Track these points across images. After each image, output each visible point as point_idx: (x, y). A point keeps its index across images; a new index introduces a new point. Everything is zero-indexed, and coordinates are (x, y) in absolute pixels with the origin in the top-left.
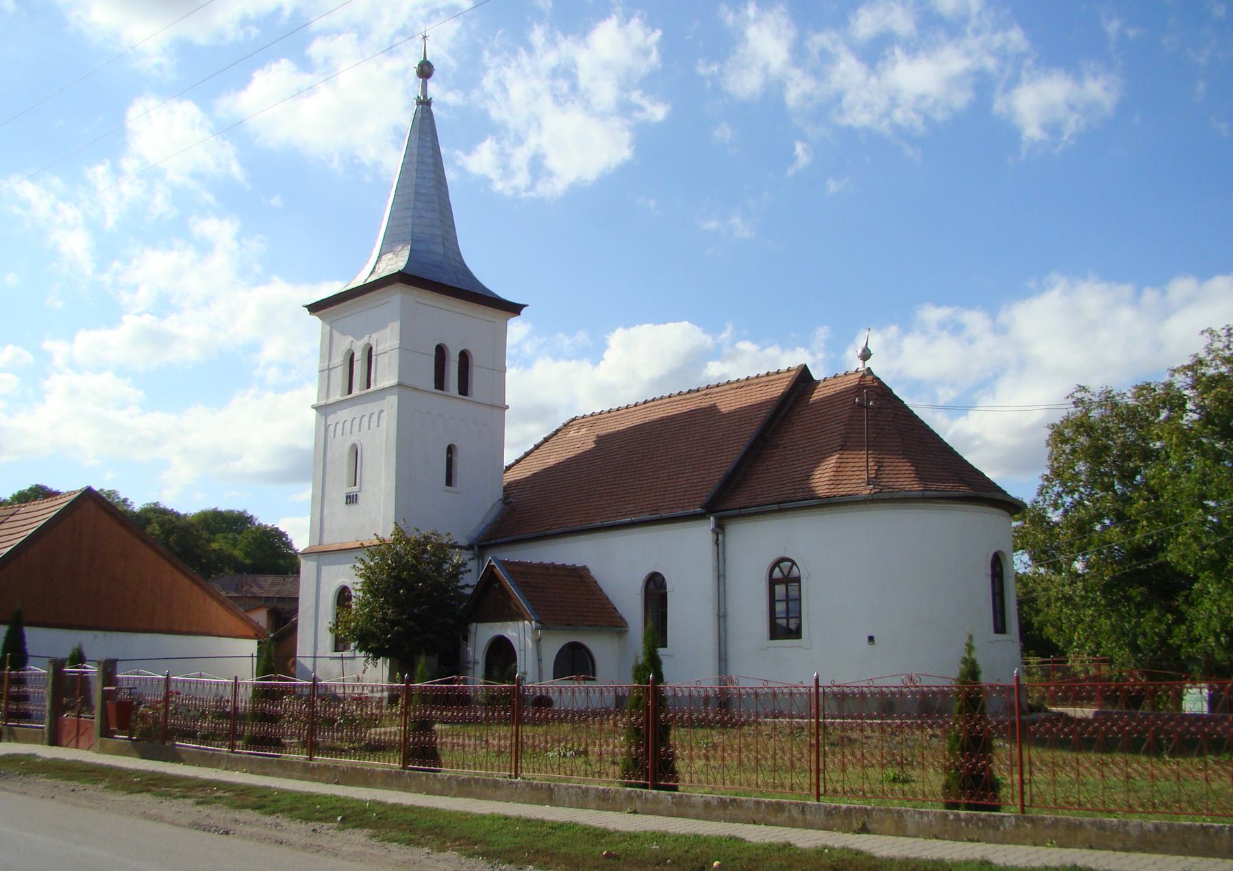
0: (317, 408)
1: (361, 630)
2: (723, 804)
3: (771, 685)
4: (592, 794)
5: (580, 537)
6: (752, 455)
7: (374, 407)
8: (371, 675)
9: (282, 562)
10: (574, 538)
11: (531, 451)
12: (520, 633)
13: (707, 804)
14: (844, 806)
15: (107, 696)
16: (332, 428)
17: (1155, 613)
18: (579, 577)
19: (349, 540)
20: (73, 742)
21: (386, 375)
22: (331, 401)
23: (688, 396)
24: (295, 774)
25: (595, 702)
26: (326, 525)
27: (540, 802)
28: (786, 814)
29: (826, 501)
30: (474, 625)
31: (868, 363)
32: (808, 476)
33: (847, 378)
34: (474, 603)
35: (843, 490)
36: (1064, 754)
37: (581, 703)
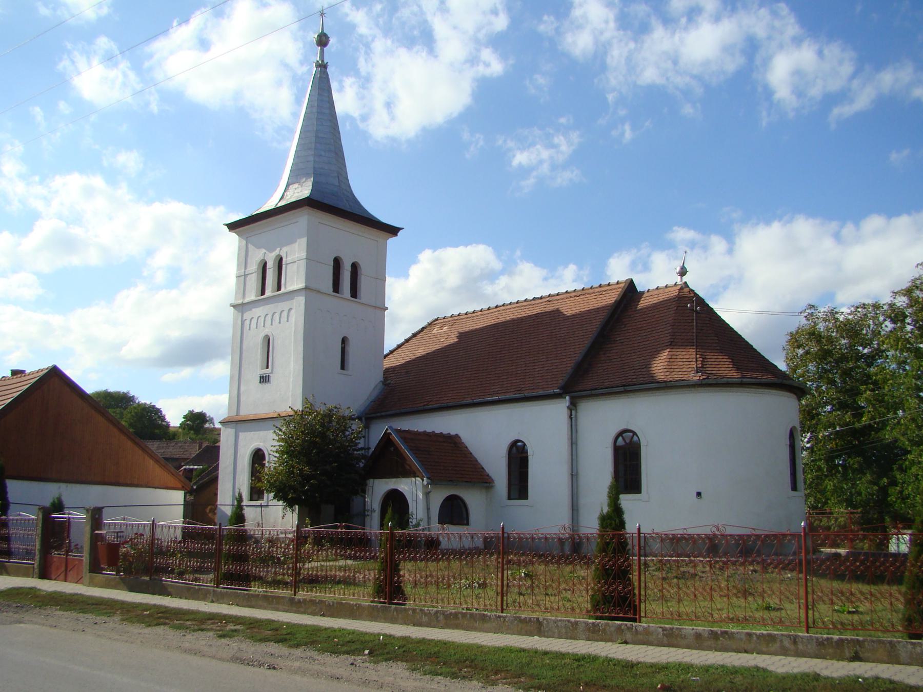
0: (234, 306)
1: (281, 482)
2: (714, 635)
4: (581, 627)
5: (452, 412)
6: (613, 344)
7: (284, 305)
8: (276, 519)
9: (157, 431)
10: (472, 409)
11: (403, 344)
12: (412, 488)
13: (698, 636)
14: (836, 637)
15: (95, 539)
16: (247, 322)
17: (869, 477)
18: (453, 442)
19: (263, 411)
20: (62, 576)
21: (295, 280)
22: (247, 300)
23: (533, 302)
24: (281, 607)
25: (467, 543)
26: (243, 399)
27: (530, 634)
28: (778, 644)
29: (663, 385)
30: (372, 480)
31: (685, 279)
32: (647, 366)
33: (667, 290)
34: (369, 466)
35: (676, 376)
36: (860, 586)
37: (455, 544)
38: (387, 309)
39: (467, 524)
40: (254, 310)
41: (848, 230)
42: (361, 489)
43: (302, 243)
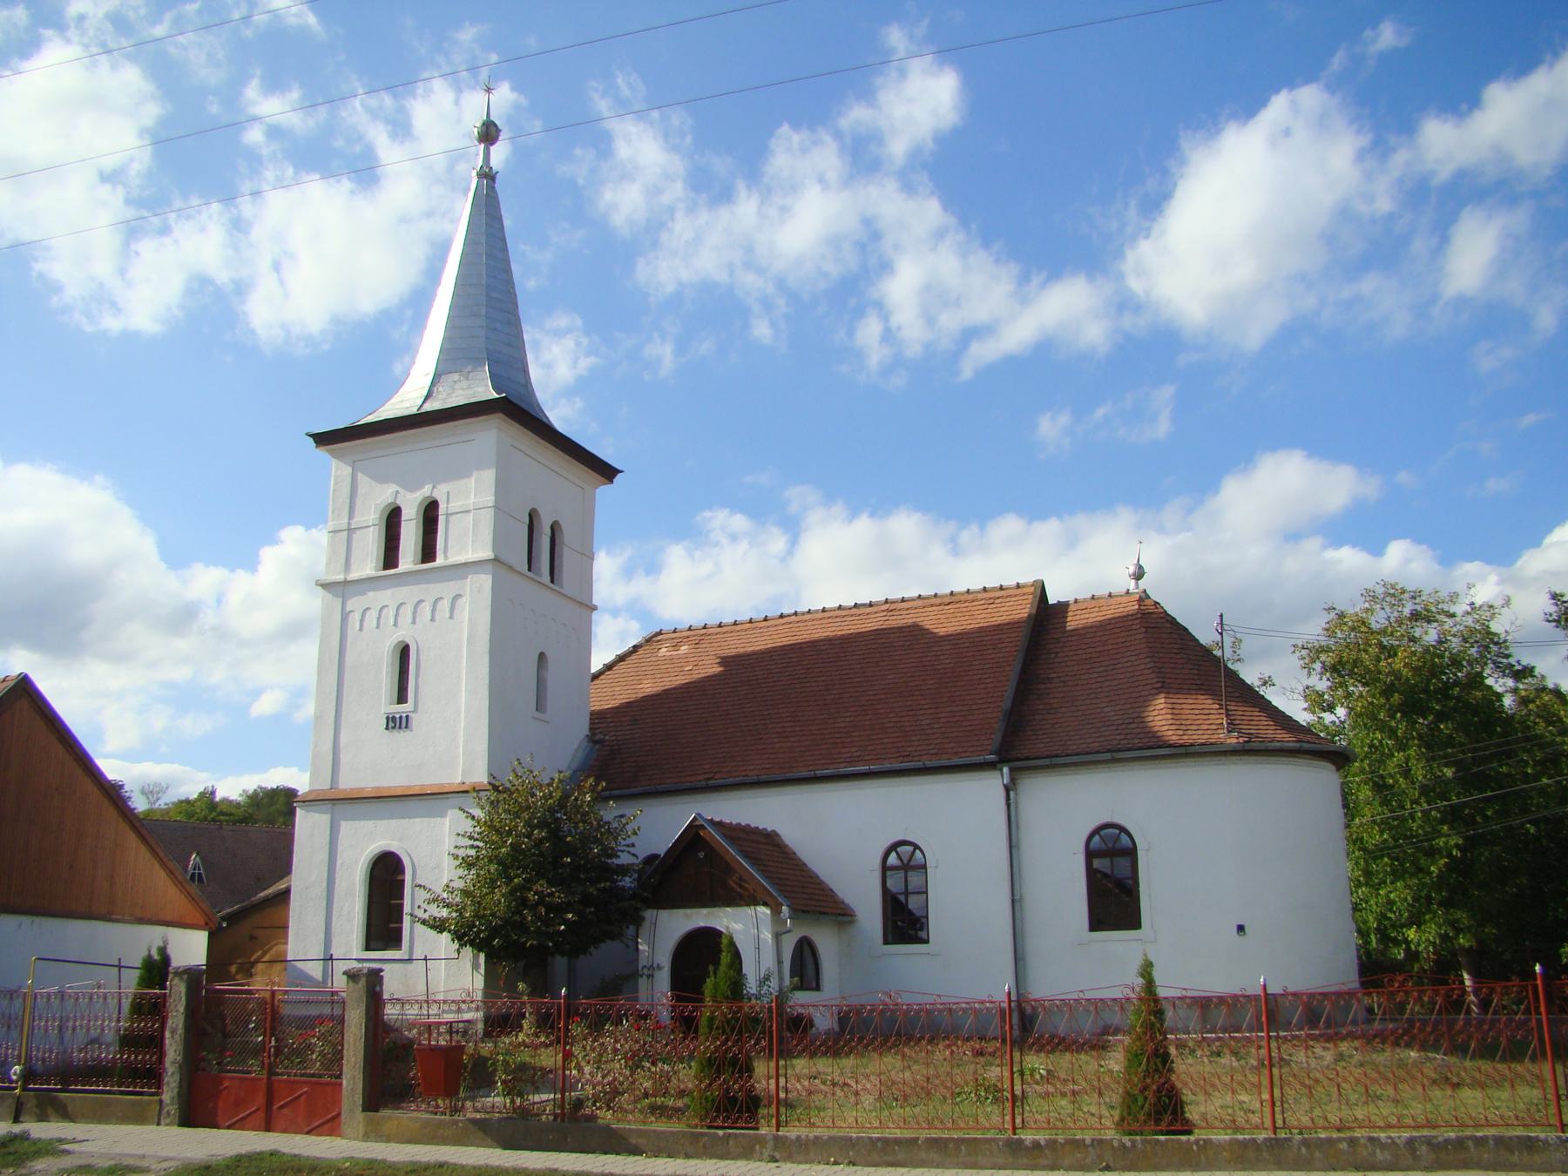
3: (944, 1000)
6: (1040, 689)
7: (446, 589)
16: (356, 616)
26: (344, 758)
29: (1182, 750)
32: (1140, 720)
33: (1112, 601)
38: (595, 608)
39: (818, 988)
40: (371, 594)
41: (966, 536)
43: (488, 477)
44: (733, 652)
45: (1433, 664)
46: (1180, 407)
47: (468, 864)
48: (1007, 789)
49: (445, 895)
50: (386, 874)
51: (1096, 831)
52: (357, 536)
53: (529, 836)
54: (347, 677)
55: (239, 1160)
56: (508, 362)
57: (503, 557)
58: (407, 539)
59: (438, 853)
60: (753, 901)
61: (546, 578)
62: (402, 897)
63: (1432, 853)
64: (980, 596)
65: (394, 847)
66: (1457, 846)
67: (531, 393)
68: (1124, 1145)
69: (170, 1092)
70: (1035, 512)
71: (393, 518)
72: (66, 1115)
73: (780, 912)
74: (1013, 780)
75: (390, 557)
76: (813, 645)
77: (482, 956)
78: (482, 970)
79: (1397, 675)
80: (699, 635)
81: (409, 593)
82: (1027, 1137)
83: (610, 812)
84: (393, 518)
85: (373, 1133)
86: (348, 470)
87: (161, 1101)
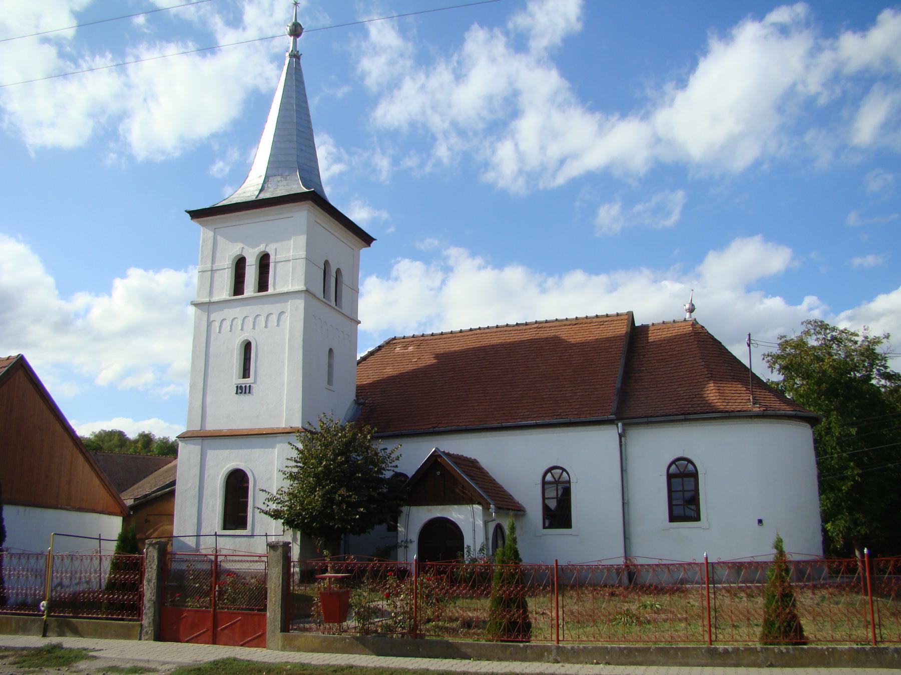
6: (644, 375)
7: (275, 308)
16: (216, 324)
22: (215, 299)
29: (727, 414)
33: (676, 325)
38: (359, 322)
40: (226, 310)
41: (550, 282)
42: (392, 518)
43: (302, 240)
44: (442, 351)
45: (844, 367)
46: (694, 206)
47: (292, 477)
48: (620, 436)
49: (279, 496)
50: (237, 485)
51: (673, 462)
52: (217, 275)
53: (334, 460)
54: (211, 361)
55: (216, 663)
56: (308, 169)
57: (312, 290)
58: (250, 277)
59: (272, 471)
60: (470, 501)
61: (333, 303)
62: (247, 497)
63: (844, 479)
64: (594, 320)
65: (242, 466)
66: (858, 474)
67: (323, 191)
68: (781, 651)
69: (147, 620)
70: (593, 269)
71: (240, 264)
72: (76, 632)
73: (489, 509)
74: (624, 430)
75: (238, 287)
76: (494, 348)
77: (299, 534)
78: (299, 543)
79: (824, 372)
80: (420, 341)
81: (250, 310)
82: (721, 646)
83: (379, 446)
84: (240, 264)
85: (288, 646)
86: (211, 234)
87: (141, 625)
